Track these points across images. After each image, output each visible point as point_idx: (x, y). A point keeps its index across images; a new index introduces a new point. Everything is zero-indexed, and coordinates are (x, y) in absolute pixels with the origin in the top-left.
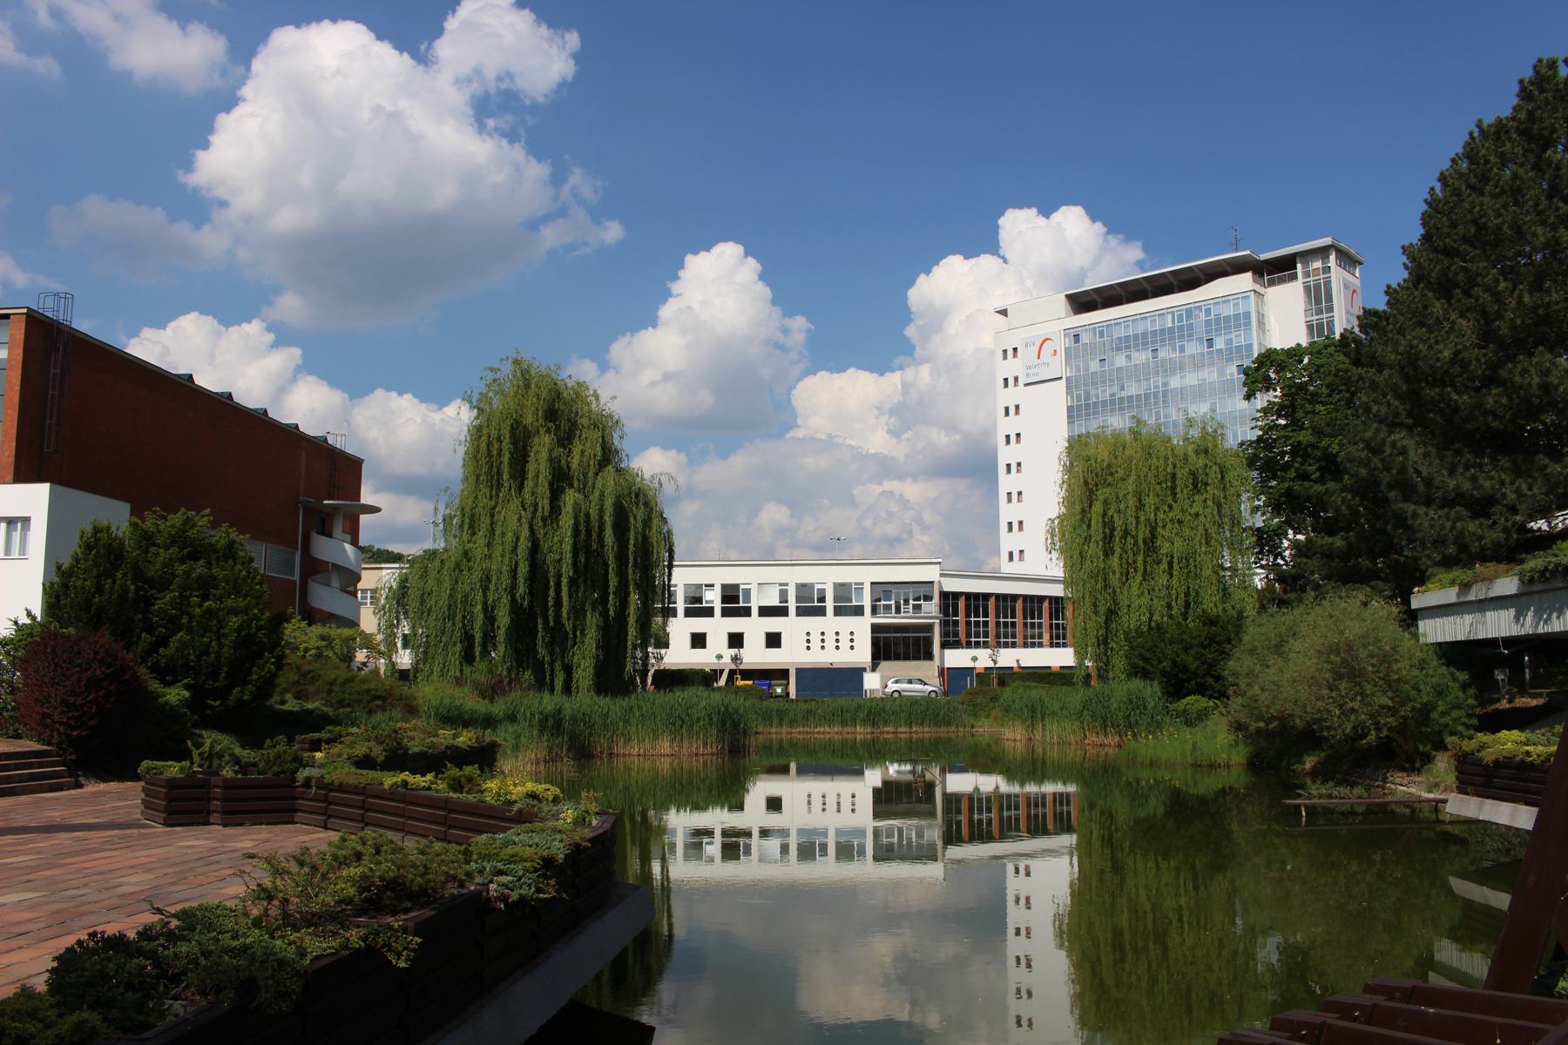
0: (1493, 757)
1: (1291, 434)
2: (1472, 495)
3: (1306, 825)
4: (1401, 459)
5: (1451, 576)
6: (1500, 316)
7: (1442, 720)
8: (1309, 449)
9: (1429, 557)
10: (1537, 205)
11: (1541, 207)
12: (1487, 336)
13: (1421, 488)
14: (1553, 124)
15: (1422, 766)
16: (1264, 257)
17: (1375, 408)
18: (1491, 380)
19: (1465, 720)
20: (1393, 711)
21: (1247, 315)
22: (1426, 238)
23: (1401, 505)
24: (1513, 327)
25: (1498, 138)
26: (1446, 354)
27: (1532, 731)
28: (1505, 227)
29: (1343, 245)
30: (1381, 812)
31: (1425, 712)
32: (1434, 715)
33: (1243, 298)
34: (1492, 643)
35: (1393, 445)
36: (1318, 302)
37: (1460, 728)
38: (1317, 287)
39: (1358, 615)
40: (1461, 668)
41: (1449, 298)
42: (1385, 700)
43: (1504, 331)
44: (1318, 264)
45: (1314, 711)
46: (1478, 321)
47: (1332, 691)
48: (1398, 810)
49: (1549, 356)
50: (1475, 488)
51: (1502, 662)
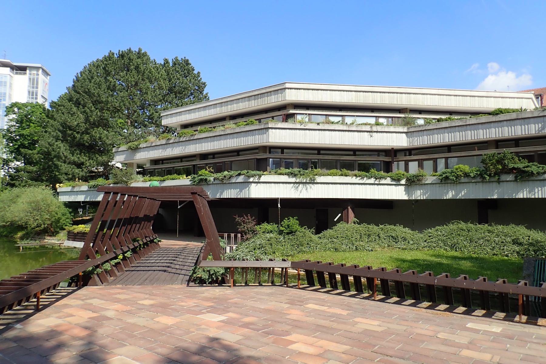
0: (77, 231)
1: (20, 131)
2: (78, 162)
3: (22, 252)
4: (59, 149)
5: (70, 184)
6: (91, 116)
7: (63, 222)
8: (26, 136)
9: (64, 177)
10: (104, 90)
11: (105, 91)
12: (87, 120)
13: (64, 158)
14: (111, 70)
15: (56, 235)
16: (15, 64)
17: (52, 133)
18: (86, 132)
19: (69, 222)
20: (49, 220)
21: (5, 82)
22: (74, 86)
23: (57, 162)
24: (94, 120)
25: (97, 68)
26: (75, 123)
27: (87, 225)
28: (96, 93)
29: (44, 68)
30: (43, 247)
31: (58, 220)
32: (61, 221)
33: (5, 76)
34: (79, 202)
35: (57, 145)
36: (33, 84)
37: (68, 224)
38: (34, 79)
39: (41, 193)
40: (70, 208)
41: (78, 107)
42: (47, 217)
43: (92, 120)
44: (35, 72)
45: (25, 219)
46: (85, 116)
47: (31, 214)
48: (49, 247)
49: (102, 130)
50: (79, 160)
51: (81, 207)
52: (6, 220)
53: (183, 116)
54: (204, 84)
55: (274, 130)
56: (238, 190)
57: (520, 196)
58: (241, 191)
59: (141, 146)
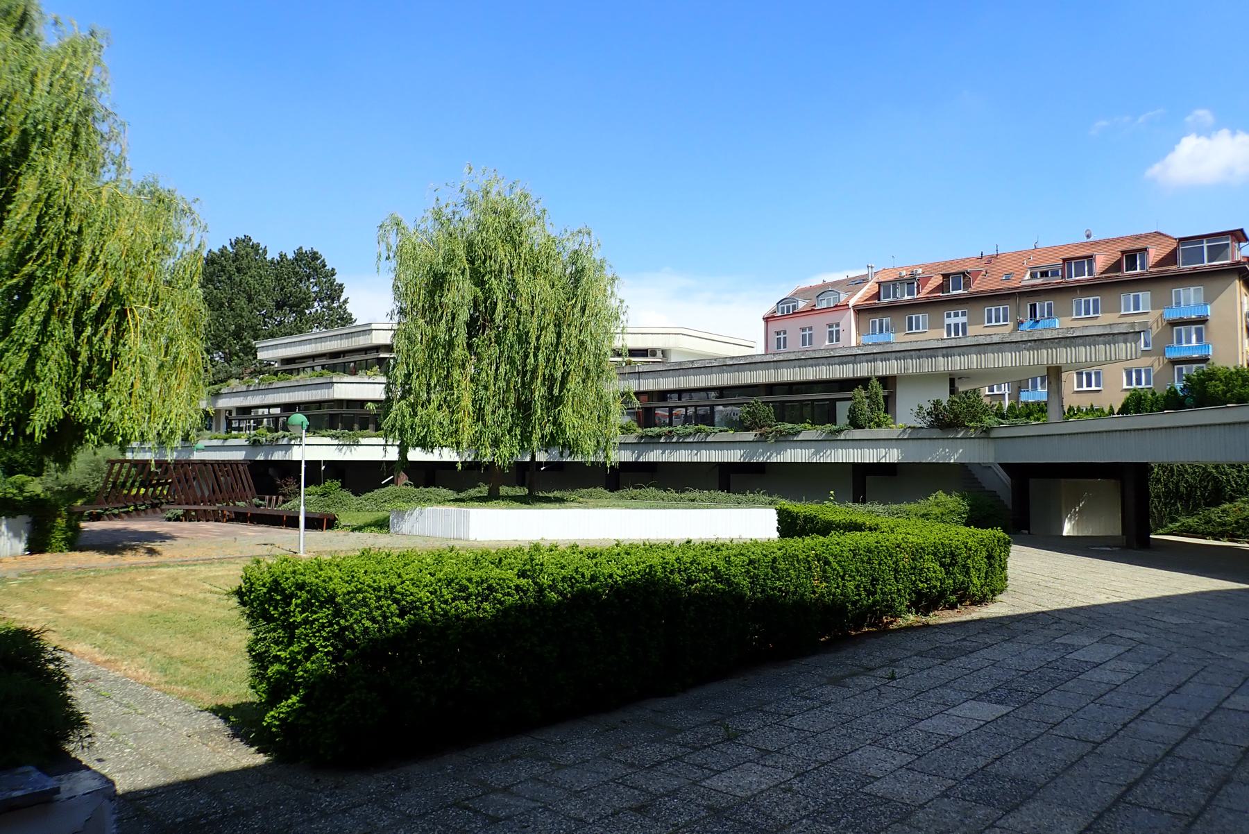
52: (63, 483)
53: (289, 349)
54: (341, 285)
55: (339, 385)
56: (813, 450)
57: (274, 458)
58: (664, 452)
59: (222, 391)
